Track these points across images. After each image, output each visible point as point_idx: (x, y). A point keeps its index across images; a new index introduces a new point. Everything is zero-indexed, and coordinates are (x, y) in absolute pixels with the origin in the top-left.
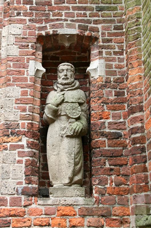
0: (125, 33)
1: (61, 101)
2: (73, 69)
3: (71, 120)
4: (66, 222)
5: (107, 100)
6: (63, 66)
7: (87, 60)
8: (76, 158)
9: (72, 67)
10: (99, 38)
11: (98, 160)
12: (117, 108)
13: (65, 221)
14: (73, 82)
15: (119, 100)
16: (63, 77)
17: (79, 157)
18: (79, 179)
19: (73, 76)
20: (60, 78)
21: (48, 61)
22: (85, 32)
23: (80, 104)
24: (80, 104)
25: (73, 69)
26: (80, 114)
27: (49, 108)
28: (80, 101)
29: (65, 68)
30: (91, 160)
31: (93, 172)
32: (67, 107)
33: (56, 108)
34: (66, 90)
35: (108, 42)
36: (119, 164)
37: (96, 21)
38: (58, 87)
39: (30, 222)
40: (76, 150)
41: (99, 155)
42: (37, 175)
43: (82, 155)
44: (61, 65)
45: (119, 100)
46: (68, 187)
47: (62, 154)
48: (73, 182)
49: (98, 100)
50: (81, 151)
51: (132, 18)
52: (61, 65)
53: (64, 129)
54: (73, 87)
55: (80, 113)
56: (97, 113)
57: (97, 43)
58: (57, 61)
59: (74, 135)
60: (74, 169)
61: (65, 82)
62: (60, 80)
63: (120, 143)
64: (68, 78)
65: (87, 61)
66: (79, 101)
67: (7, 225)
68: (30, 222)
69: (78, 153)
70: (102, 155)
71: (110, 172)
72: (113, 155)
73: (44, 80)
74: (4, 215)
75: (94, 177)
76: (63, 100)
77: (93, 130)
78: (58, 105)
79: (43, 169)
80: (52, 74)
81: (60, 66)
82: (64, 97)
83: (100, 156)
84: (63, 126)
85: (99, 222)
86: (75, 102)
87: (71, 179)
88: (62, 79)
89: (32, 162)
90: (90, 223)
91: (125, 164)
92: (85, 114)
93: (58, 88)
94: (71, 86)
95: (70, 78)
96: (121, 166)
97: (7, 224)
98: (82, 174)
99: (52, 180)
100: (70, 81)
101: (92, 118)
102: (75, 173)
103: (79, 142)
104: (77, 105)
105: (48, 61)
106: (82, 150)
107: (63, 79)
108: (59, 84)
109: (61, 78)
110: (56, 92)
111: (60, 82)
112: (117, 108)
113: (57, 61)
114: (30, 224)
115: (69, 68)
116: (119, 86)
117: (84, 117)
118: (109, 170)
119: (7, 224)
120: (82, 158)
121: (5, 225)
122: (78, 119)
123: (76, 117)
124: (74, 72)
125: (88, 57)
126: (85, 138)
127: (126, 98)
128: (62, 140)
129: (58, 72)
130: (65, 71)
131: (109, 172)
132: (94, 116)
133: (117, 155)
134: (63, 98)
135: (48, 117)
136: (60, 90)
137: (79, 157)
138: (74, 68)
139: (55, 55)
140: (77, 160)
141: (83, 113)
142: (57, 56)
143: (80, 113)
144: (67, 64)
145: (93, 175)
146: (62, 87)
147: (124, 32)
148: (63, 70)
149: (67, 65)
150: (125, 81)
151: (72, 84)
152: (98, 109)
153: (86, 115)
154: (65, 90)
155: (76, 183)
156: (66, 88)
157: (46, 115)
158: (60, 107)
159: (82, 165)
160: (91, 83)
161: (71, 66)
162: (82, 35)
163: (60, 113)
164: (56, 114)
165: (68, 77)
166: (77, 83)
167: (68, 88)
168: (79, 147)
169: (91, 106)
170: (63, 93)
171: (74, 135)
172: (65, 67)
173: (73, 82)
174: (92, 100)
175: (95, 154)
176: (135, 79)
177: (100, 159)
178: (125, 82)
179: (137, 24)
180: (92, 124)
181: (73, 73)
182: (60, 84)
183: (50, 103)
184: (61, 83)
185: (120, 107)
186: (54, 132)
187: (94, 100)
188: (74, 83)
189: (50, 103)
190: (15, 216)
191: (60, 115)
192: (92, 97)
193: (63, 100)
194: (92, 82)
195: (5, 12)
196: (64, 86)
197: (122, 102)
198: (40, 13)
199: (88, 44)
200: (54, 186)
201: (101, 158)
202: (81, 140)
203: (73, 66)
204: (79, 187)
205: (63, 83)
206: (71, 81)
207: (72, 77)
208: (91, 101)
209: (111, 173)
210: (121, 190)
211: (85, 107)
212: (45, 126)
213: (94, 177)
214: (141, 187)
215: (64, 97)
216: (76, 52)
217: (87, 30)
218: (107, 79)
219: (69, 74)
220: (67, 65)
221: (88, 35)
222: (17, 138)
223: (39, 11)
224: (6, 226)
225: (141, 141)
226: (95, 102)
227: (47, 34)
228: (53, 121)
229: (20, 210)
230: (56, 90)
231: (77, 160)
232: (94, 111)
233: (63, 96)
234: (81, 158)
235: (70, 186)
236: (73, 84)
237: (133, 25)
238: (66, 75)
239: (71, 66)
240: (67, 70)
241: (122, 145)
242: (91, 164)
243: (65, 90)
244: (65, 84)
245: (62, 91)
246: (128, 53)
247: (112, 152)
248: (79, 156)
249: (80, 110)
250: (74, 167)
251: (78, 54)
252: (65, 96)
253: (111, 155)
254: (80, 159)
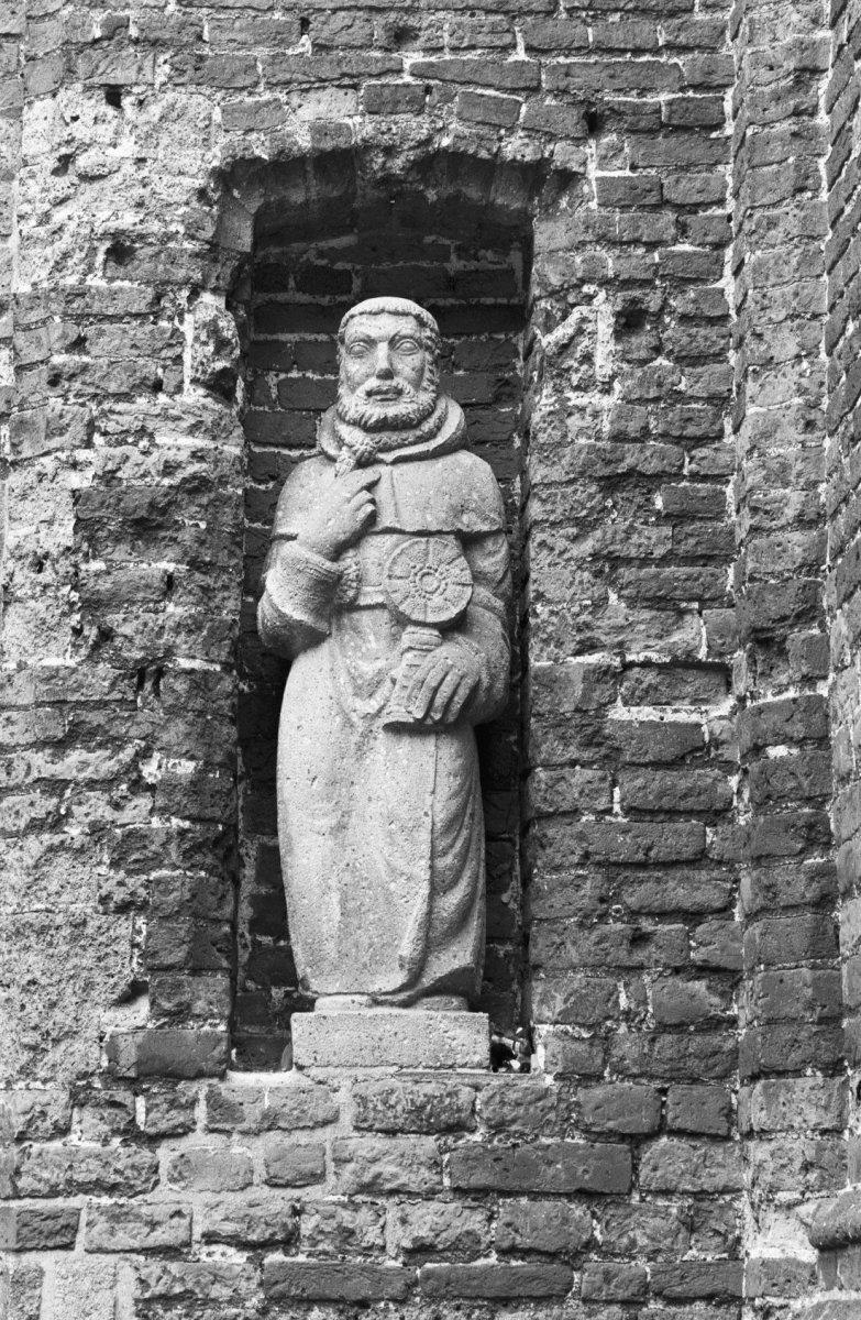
0: (733, 147)
1: (358, 525)
2: (428, 333)
3: (410, 636)
4: (383, 1227)
5: (621, 541)
6: (373, 321)
7: (511, 296)
8: (445, 853)
9: (421, 323)
10: (583, 174)
11: (564, 885)
12: (676, 588)
13: (375, 1222)
14: (426, 414)
15: (692, 541)
16: (373, 383)
17: (459, 844)
18: (456, 964)
19: (427, 375)
20: (353, 390)
21: (281, 297)
22: (500, 139)
23: (469, 542)
24: (469, 542)
25: (428, 333)
26: (464, 603)
27: (296, 567)
28: (471, 522)
29: (382, 325)
30: (526, 880)
31: (535, 946)
32: (394, 562)
33: (328, 565)
34: (389, 457)
35: (619, 633)
36: (687, 904)
37: (567, 75)
38: (341, 443)
39: (185, 1222)
40: (438, 806)
41: (573, 853)
42: (225, 964)
43: (480, 829)
44: (361, 314)
45: (692, 541)
46: (396, 1011)
47: (363, 815)
48: (426, 981)
49: (575, 539)
50: (469, 811)
51: (771, 68)
52: (361, 314)
53: (368, 688)
54: (427, 440)
55: (469, 590)
56: (564, 617)
57: (571, 204)
58: (344, 298)
59: (429, 722)
60: (430, 913)
61: (375, 412)
62: (353, 402)
63: (690, 789)
64: (399, 392)
65: (515, 301)
66: (460, 526)
67: (59, 1240)
68: (185, 1222)
69: (453, 823)
70: (587, 855)
71: (630, 953)
72: (652, 854)
73: (271, 485)
74: (40, 1186)
75: (542, 975)
76: (372, 518)
77: (541, 710)
78: (338, 551)
79: (256, 925)
80: (309, 375)
81: (352, 317)
82: (373, 501)
83: (576, 859)
84: (368, 669)
85: (566, 1221)
86: (440, 533)
87: (418, 968)
88: (363, 395)
89: (194, 896)
90: (517, 1231)
91: (717, 905)
92: (493, 599)
93: (340, 449)
94: (418, 433)
95: (408, 388)
96: (698, 918)
97: (57, 1233)
98: (479, 939)
99: (309, 970)
100: (412, 407)
101: (535, 645)
102: (432, 938)
103: (460, 761)
104: (451, 547)
105: (281, 297)
106: (476, 806)
107: (369, 394)
108: (349, 423)
109: (361, 392)
110: (330, 471)
111: (352, 414)
112: (676, 588)
113: (344, 298)
114: (182, 1235)
115: (404, 332)
116: (692, 458)
117: (488, 614)
118: (625, 942)
119: (57, 1233)
120: (473, 847)
121: (47, 1238)
122: (452, 629)
123: (445, 616)
124: (432, 353)
125: (519, 274)
126: (494, 738)
127: (731, 533)
128: (361, 750)
129: (343, 350)
130: (383, 348)
131: (623, 954)
132: (550, 629)
133: (674, 857)
134: (370, 508)
135: (282, 615)
136: (352, 462)
137: (459, 844)
138: (432, 330)
139: (324, 262)
140: (449, 860)
141: (484, 593)
142: (339, 266)
143: (469, 590)
144: (392, 308)
145: (537, 967)
146: (360, 440)
147: (728, 138)
148: (371, 342)
149: (396, 313)
150: (728, 429)
151: (420, 423)
152: (572, 591)
153: (499, 604)
154: (381, 462)
155: (443, 988)
156: (388, 449)
157: (273, 606)
158: (349, 562)
159: (475, 888)
160: (535, 438)
161: (417, 317)
162: (483, 154)
163: (351, 593)
164: (333, 600)
165: (398, 381)
166: (454, 418)
167: (400, 446)
168: (462, 786)
169: (533, 575)
170: (367, 475)
171: (429, 722)
172: (385, 327)
173: (426, 414)
174: (538, 540)
175: (549, 851)
176: (777, 425)
177: (579, 876)
178: (729, 439)
179: (796, 107)
180: (535, 678)
181: (429, 357)
182: (355, 423)
183: (292, 538)
184: (356, 416)
185: (697, 579)
186: (310, 694)
187: (550, 541)
188: (437, 414)
189: (292, 538)
190: (98, 1186)
191: (353, 607)
192: (536, 523)
193: (372, 518)
194: (540, 435)
195: (32, 13)
196: (377, 437)
197: (708, 552)
198: (237, 24)
199: (516, 205)
200: (317, 1004)
201: (581, 872)
202: (472, 746)
203: (427, 315)
204: (457, 1014)
205: (371, 416)
206: (415, 407)
207: (425, 384)
208: (532, 546)
209: (639, 956)
210: (691, 1050)
211: (493, 560)
212: (263, 664)
213: (542, 975)
214: (796, 1041)
215: (373, 501)
216: (448, 242)
217: (511, 130)
218: (623, 422)
219: (407, 365)
220: (396, 313)
221: (519, 157)
222: (110, 758)
223: (235, 13)
224: (50, 1244)
225: (806, 783)
226: (552, 549)
227: (281, 152)
228: (315, 639)
229: (130, 1161)
230: (332, 460)
231: (449, 860)
232: (549, 602)
233: (366, 495)
234: (467, 851)
235: (406, 1004)
236: (427, 427)
237: (774, 111)
238: (388, 374)
239: (417, 317)
240: (393, 342)
241: (702, 798)
242: (523, 907)
243: (381, 462)
244: (383, 425)
245: (363, 462)
246: (745, 269)
247: (648, 842)
248: (455, 839)
249: (467, 577)
250: (432, 897)
251: (462, 252)
252: (382, 493)
253: (640, 856)
254: (463, 857)
